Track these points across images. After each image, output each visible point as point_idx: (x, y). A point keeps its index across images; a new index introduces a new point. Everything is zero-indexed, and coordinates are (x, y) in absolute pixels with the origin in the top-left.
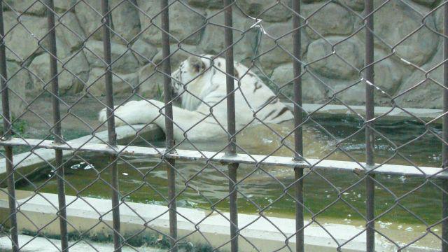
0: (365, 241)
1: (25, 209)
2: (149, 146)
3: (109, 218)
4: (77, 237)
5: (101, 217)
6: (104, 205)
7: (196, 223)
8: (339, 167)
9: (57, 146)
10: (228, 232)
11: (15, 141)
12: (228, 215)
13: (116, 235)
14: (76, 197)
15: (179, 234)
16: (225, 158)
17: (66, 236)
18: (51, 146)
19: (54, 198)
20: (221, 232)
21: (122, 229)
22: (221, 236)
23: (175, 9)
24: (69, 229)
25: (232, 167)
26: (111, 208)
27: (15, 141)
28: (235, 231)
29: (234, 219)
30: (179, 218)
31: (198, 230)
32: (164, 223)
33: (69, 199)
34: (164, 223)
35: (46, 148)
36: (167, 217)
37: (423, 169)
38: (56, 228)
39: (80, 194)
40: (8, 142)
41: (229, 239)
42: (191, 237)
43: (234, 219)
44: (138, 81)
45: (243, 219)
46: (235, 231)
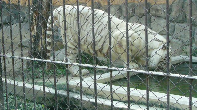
0: (166, 98)
1: (104, 90)
2: (90, 64)
3: (145, 97)
4: (152, 105)
5: (143, 96)
6: (144, 92)
7: (177, 100)
8: (174, 74)
9: (128, 70)
10: (188, 104)
11: (113, 68)
12: (189, 98)
13: (148, 104)
14: (119, 87)
15: (170, 104)
16: (188, 77)
17: (129, 101)
18: (126, 70)
19: (126, 89)
20: (107, 90)
21: (149, 100)
22: (123, 95)
23: (164, 23)
24: (131, 99)
25: (191, 81)
26: (146, 93)
27: (113, 68)
28: (191, 103)
29: (191, 99)
30: (97, 86)
31: (177, 102)
32: (165, 99)
33: (131, 89)
34: (165, 99)
35: (124, 71)
36: (166, 97)
37: (181, 75)
38: (126, 99)
39: (137, 88)
40: (111, 69)
41: (189, 107)
42: (175, 105)
43: (191, 99)
44: (155, 48)
45: (114, 87)
46: (191, 103)
